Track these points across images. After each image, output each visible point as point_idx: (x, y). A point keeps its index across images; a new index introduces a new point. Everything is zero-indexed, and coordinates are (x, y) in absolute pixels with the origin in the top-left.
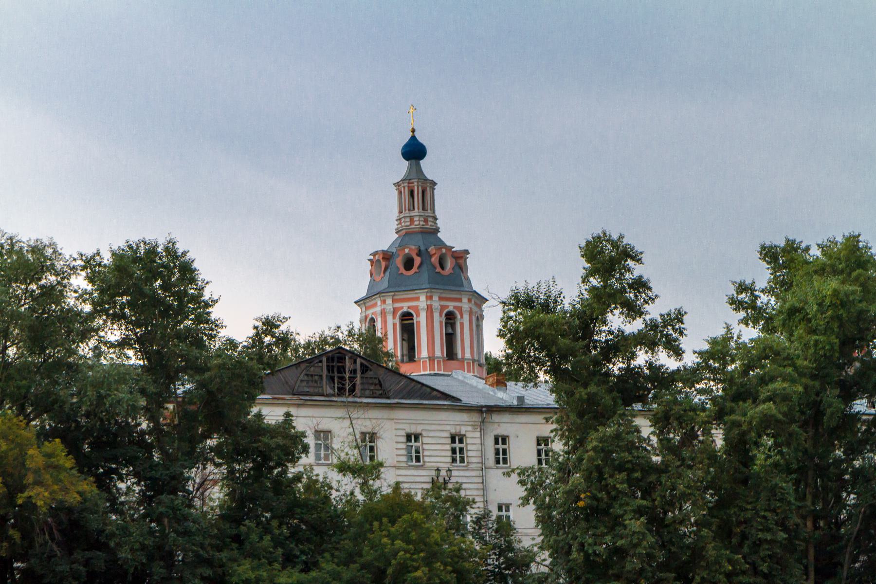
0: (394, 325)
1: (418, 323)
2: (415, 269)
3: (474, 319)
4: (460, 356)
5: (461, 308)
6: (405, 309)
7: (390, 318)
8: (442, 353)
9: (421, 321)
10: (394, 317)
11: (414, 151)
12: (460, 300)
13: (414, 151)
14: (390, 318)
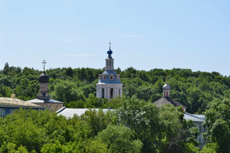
0: (101, 91)
1: (115, 91)
2: (105, 79)
3: (118, 90)
5: (115, 87)
6: (103, 88)
7: (100, 89)
8: (109, 97)
9: (105, 90)
10: (109, 89)
11: (110, 53)
12: (114, 86)
13: (110, 53)
14: (108, 89)
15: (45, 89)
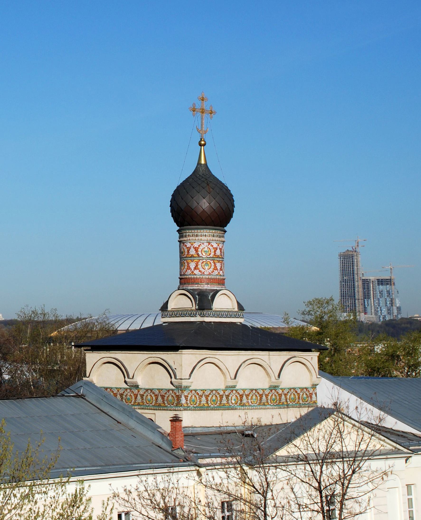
4: (188, 232)
15: (215, 268)
